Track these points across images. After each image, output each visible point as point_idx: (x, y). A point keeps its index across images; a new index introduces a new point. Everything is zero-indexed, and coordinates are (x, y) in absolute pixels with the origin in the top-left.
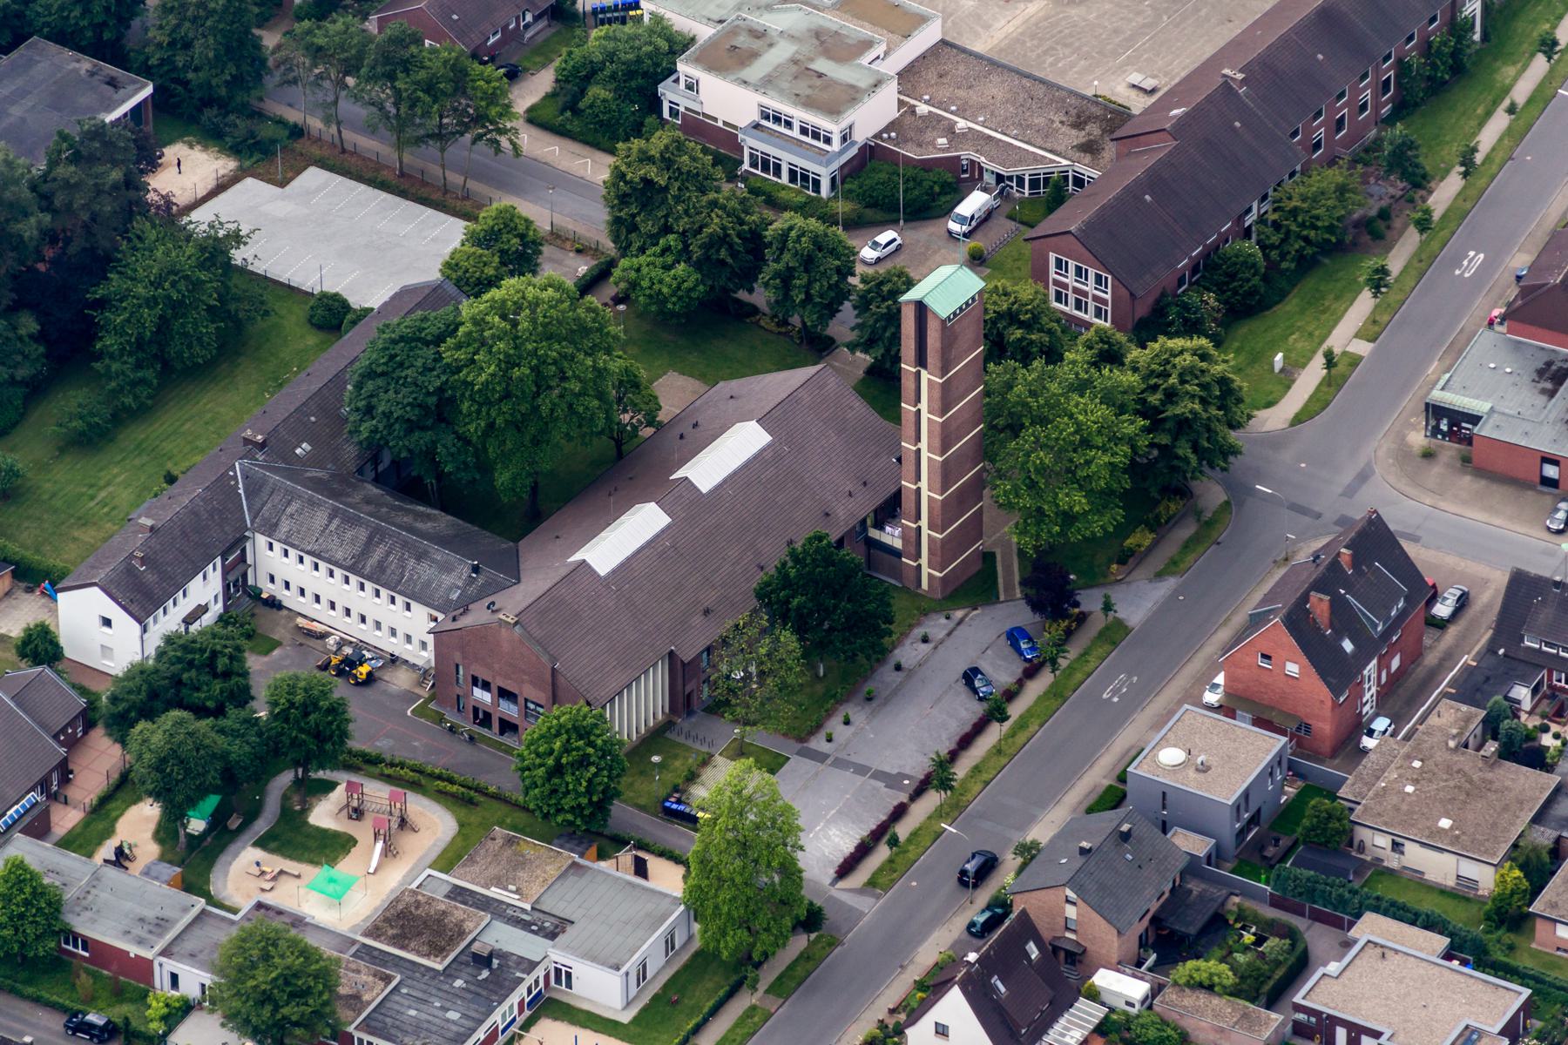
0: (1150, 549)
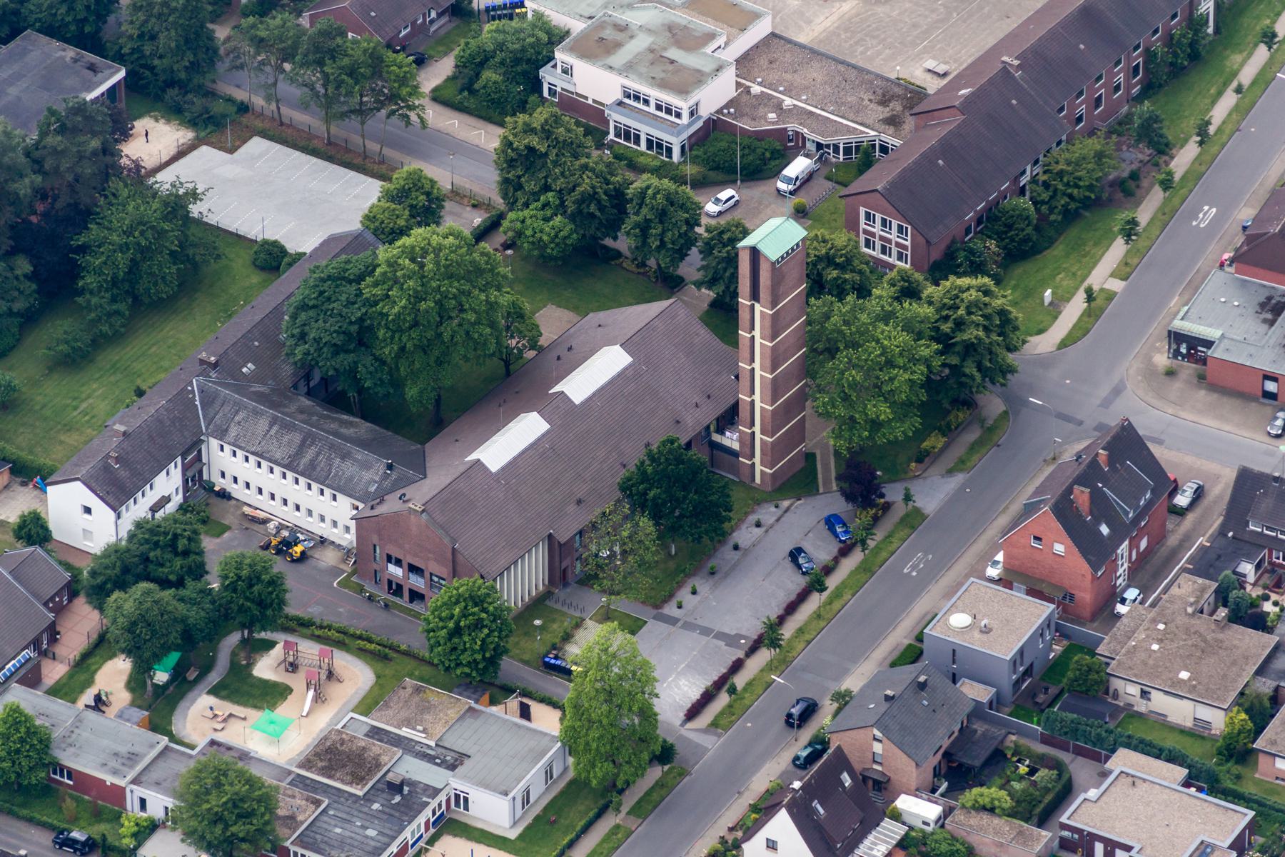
0: (943, 450)
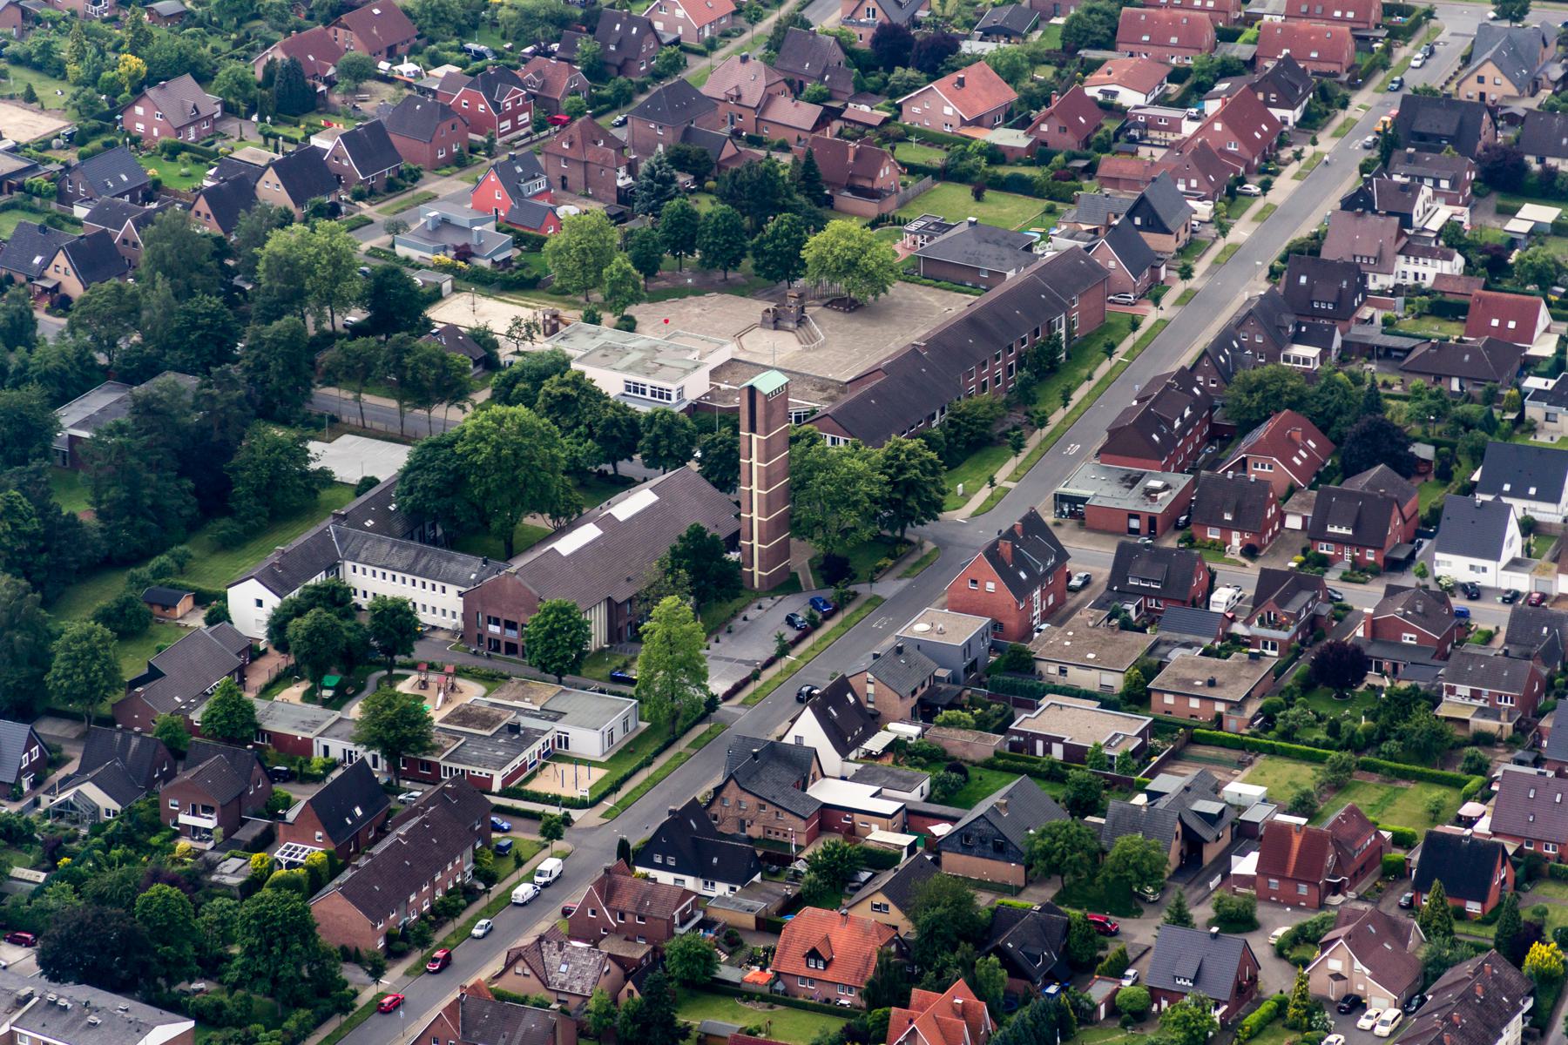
0: (892, 567)
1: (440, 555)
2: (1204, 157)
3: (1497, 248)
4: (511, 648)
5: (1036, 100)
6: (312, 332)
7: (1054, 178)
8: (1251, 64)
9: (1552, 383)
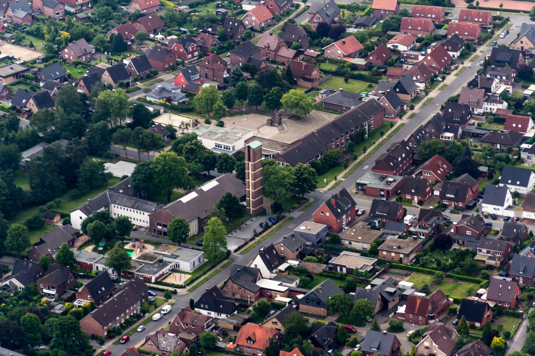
0: (298, 207)
1: (143, 202)
2: (422, 68)
3: (519, 100)
4: (165, 234)
5: (369, 49)
6: (110, 127)
7: (372, 75)
8: (445, 37)
9: (530, 146)
